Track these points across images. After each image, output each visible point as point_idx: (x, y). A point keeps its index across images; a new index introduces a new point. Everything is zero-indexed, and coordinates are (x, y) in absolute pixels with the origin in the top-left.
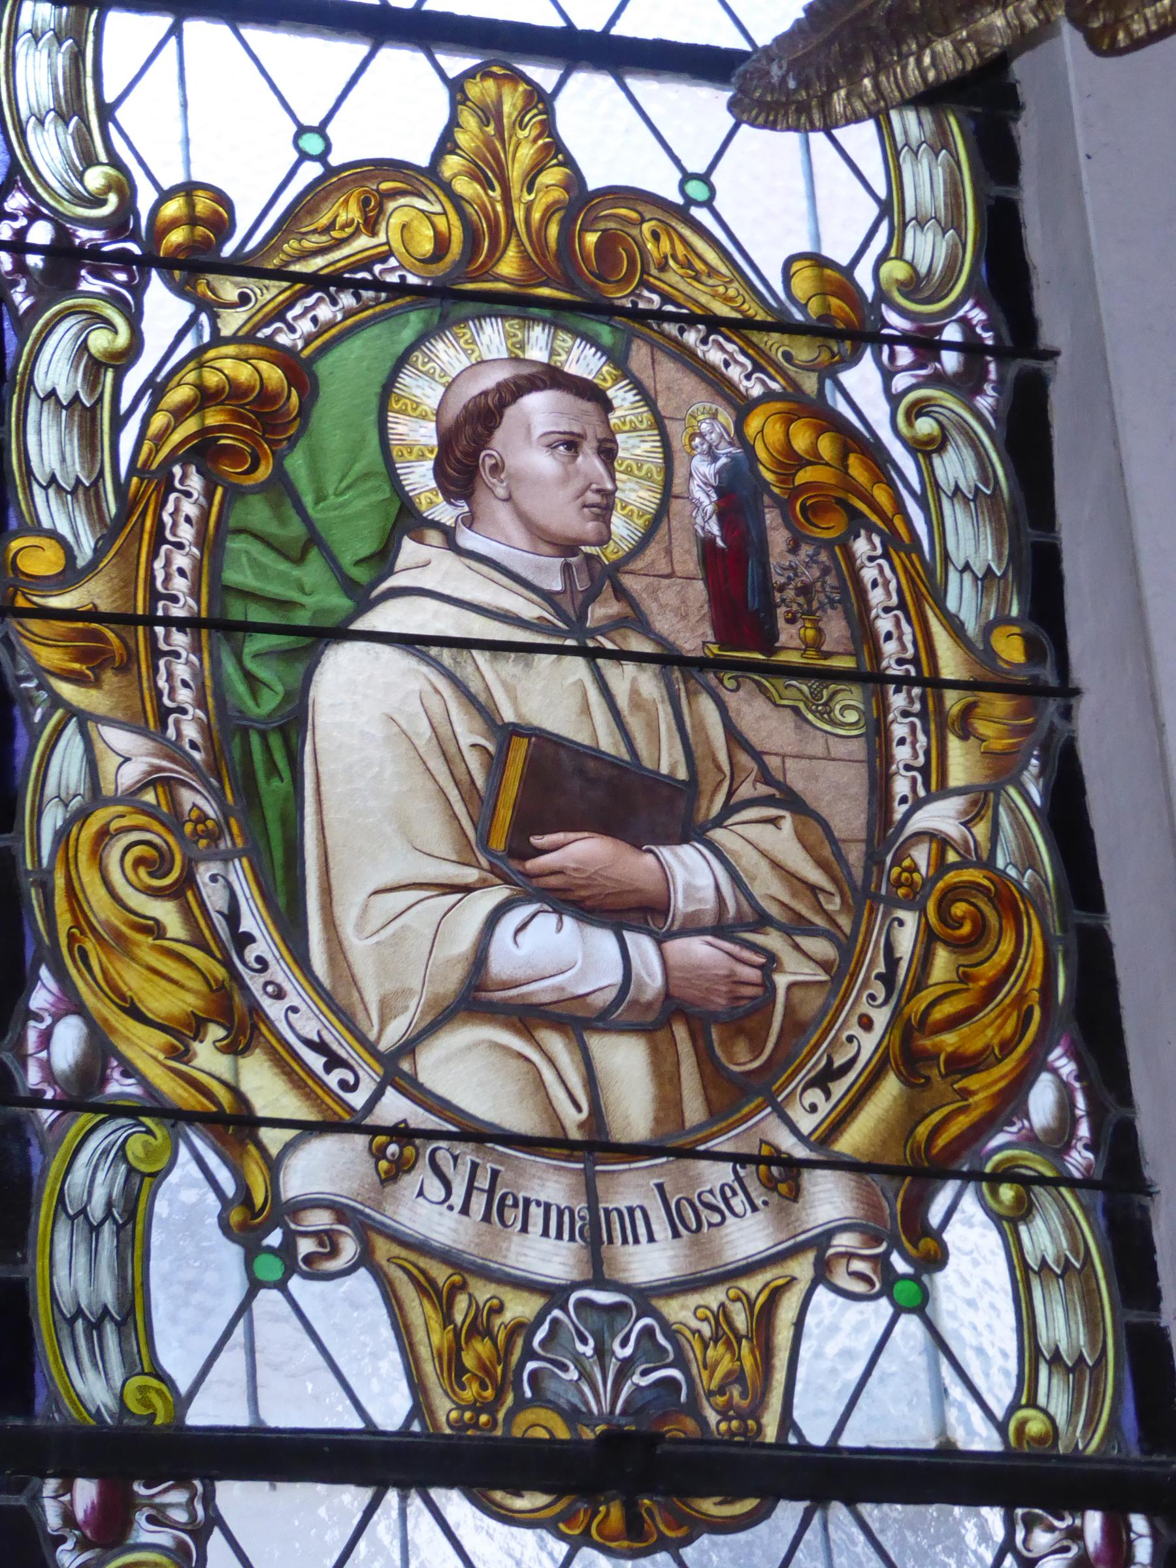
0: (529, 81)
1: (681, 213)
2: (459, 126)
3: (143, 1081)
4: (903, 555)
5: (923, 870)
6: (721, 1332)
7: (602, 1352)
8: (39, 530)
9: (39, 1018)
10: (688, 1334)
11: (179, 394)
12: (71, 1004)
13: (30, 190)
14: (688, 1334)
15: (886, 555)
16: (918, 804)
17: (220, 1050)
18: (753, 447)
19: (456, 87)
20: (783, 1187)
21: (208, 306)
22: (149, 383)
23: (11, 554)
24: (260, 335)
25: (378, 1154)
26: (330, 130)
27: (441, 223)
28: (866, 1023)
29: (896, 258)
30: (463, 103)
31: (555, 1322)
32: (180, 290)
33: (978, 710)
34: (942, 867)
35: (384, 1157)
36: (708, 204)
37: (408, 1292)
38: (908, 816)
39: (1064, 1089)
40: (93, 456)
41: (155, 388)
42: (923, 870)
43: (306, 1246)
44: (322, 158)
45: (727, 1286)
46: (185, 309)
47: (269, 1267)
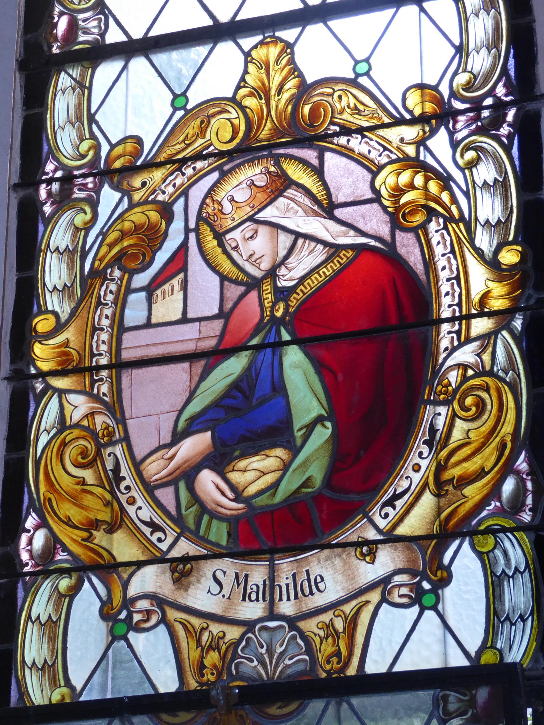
0: (282, 40)
1: (354, 83)
2: (248, 73)
3: (70, 553)
4: (454, 225)
5: (454, 386)
6: (330, 632)
7: (270, 652)
8: (47, 312)
9: (28, 531)
10: (313, 636)
11: (112, 236)
12: (43, 524)
13: (57, 160)
14: (313, 636)
15: (446, 228)
16: (454, 349)
17: (107, 533)
18: (379, 192)
19: (247, 55)
20: (368, 559)
21: (127, 193)
22: (101, 233)
23: (34, 324)
24: (150, 199)
25: (173, 571)
26: (188, 94)
27: (236, 122)
28: (417, 468)
29: (463, 72)
30: (251, 62)
31: (249, 638)
32: (116, 187)
33: (490, 294)
34: (465, 379)
35: (177, 571)
36: (367, 74)
37: (181, 632)
38: (445, 359)
39: (521, 483)
40: (72, 269)
41: (103, 234)
42: (454, 386)
43: (137, 617)
44: (184, 108)
45: (333, 610)
46: (118, 195)
47: (120, 629)
